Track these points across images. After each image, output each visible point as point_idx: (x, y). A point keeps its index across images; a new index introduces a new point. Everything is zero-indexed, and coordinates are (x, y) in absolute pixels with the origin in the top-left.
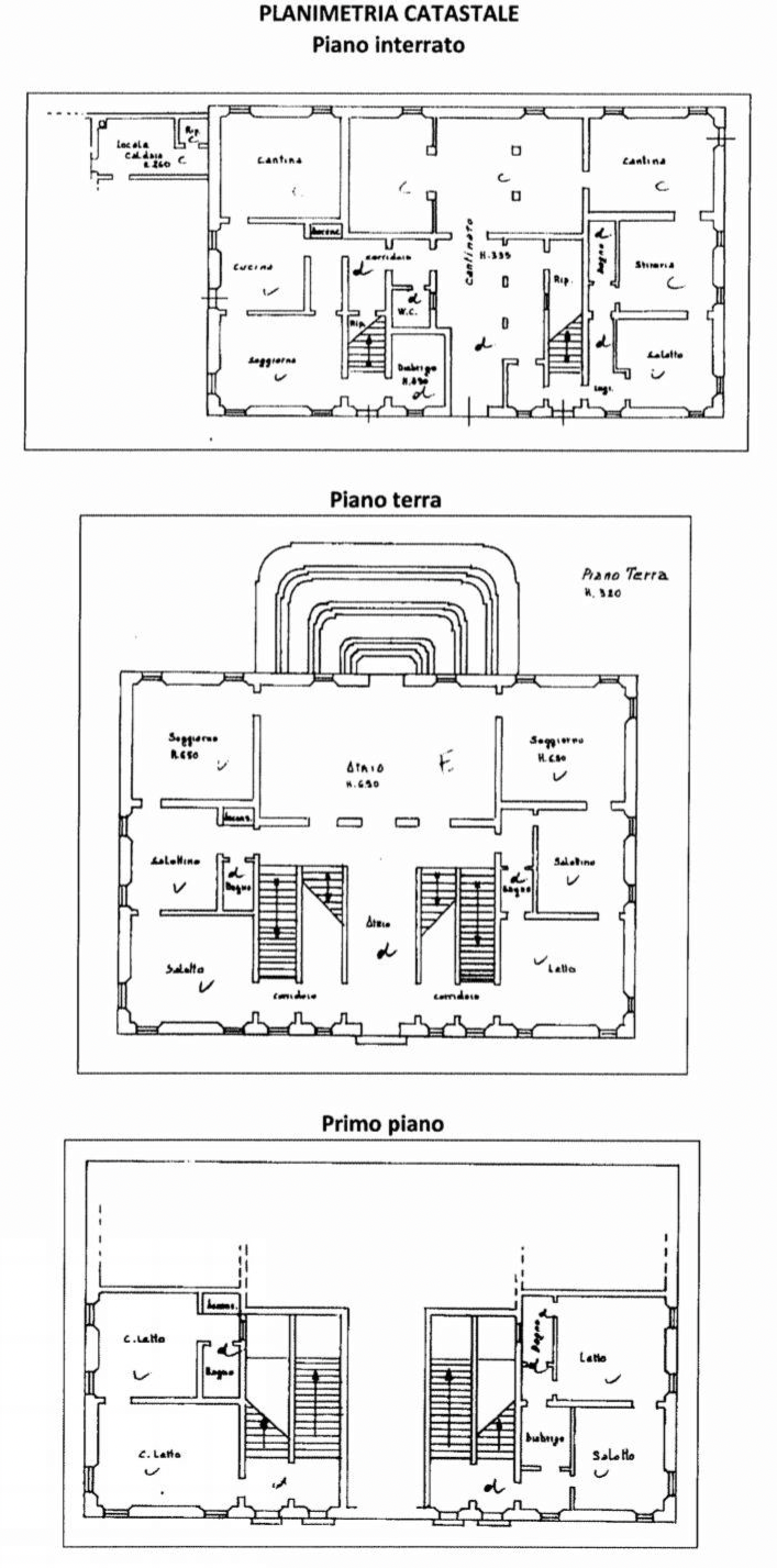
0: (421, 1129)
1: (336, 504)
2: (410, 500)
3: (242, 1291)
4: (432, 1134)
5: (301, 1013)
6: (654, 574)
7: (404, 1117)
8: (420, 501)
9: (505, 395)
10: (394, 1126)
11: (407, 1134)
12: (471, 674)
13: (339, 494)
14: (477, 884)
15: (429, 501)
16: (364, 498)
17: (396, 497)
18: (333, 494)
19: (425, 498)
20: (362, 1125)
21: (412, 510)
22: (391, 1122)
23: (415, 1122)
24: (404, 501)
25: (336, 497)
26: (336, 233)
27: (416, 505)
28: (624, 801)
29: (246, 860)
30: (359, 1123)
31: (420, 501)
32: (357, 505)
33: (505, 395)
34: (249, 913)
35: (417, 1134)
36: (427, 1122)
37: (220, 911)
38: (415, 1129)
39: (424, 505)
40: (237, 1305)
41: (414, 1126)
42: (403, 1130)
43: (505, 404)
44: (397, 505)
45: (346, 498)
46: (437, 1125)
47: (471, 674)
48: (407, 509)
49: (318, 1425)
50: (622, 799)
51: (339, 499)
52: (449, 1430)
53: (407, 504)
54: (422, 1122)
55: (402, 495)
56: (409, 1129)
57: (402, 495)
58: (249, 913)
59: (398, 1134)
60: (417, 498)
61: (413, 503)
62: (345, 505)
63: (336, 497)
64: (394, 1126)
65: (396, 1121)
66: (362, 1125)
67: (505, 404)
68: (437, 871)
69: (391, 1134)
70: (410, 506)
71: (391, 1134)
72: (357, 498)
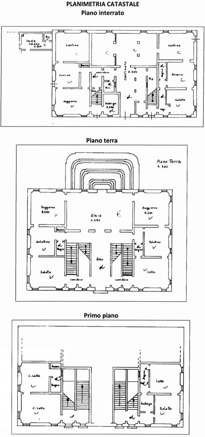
0: (112, 317)
1: (88, 142)
2: (109, 141)
3: (62, 362)
4: (115, 318)
5: (78, 285)
6: (177, 161)
7: (107, 313)
8: (112, 141)
9: (135, 111)
10: (104, 316)
11: (108, 318)
12: (126, 189)
13: (89, 139)
14: (128, 248)
15: (114, 141)
16: (96, 140)
17: (105, 140)
18: (87, 139)
19: (113, 140)
20: (95, 316)
21: (109, 143)
22: (103, 315)
23: (110, 315)
24: (107, 141)
25: (88, 140)
26: (88, 66)
27: (110, 142)
28: (169, 225)
29: (63, 242)
30: (94, 315)
31: (112, 141)
32: (94, 142)
33: (135, 111)
34: (64, 256)
35: (111, 318)
36: (113, 315)
37: (55, 256)
38: (110, 317)
39: (113, 142)
40: (60, 366)
41: (110, 316)
42: (107, 317)
43: (135, 114)
44: (105, 142)
45: (91, 140)
46: (116, 316)
47: (126, 189)
48: (108, 143)
49: (83, 400)
50: (168, 224)
51: (89, 140)
52: (120, 401)
53: (108, 142)
54: (112, 315)
55: (106, 139)
56: (108, 317)
57: (106, 139)
58: (64, 256)
59: (105, 318)
60: (111, 140)
61: (109, 141)
62: (91, 142)
63: (88, 140)
64: (104, 316)
65: (105, 315)
66: (95, 316)
67: (135, 114)
68: (116, 245)
69: (103, 318)
70: (109, 142)
71: (103, 318)
72: (94, 140)
